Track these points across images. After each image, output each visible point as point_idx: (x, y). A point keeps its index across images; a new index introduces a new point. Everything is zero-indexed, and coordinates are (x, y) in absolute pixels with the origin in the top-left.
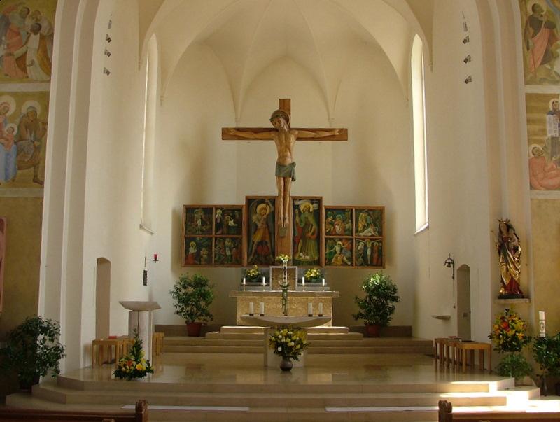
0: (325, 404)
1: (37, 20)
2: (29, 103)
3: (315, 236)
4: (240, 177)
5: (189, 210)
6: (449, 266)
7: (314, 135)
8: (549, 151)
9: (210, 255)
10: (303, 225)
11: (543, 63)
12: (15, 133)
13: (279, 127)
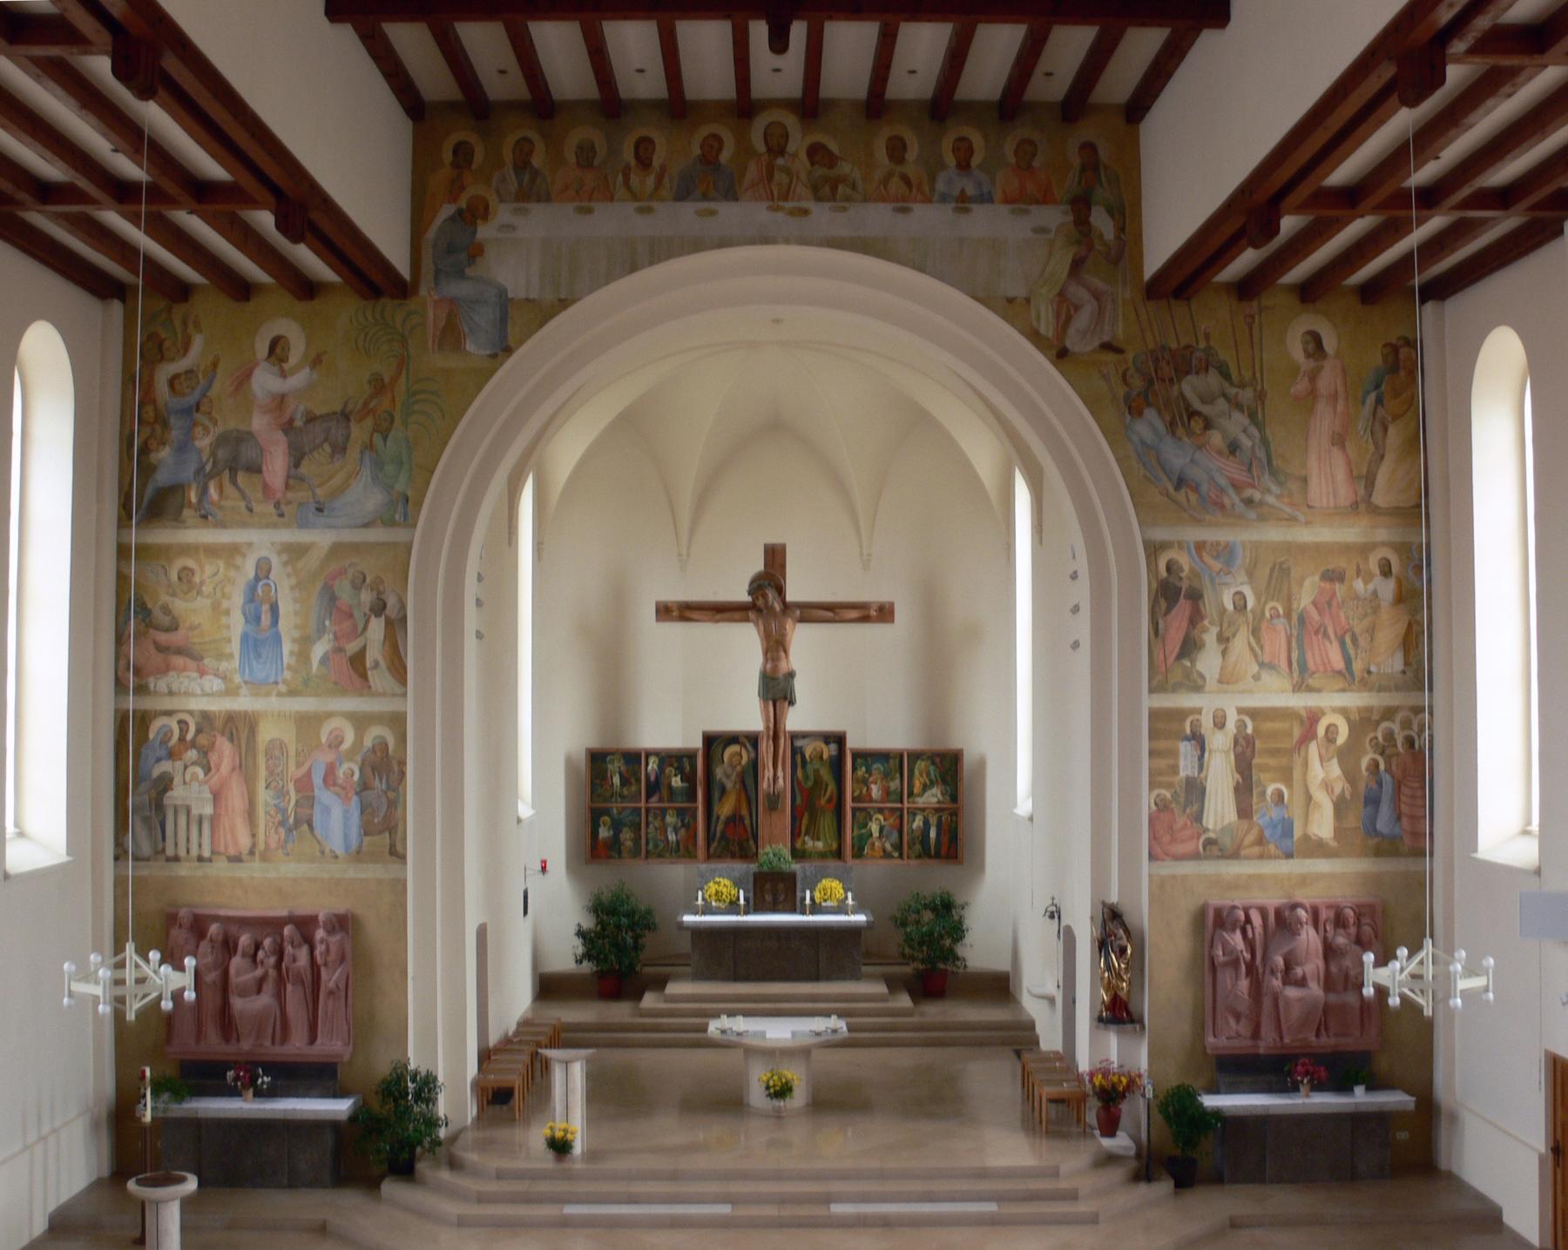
0: (828, 1199)
1: (379, 593)
4: (697, 692)
5: (597, 759)
8: (1182, 800)
9: (637, 840)
10: (810, 784)
13: (767, 602)
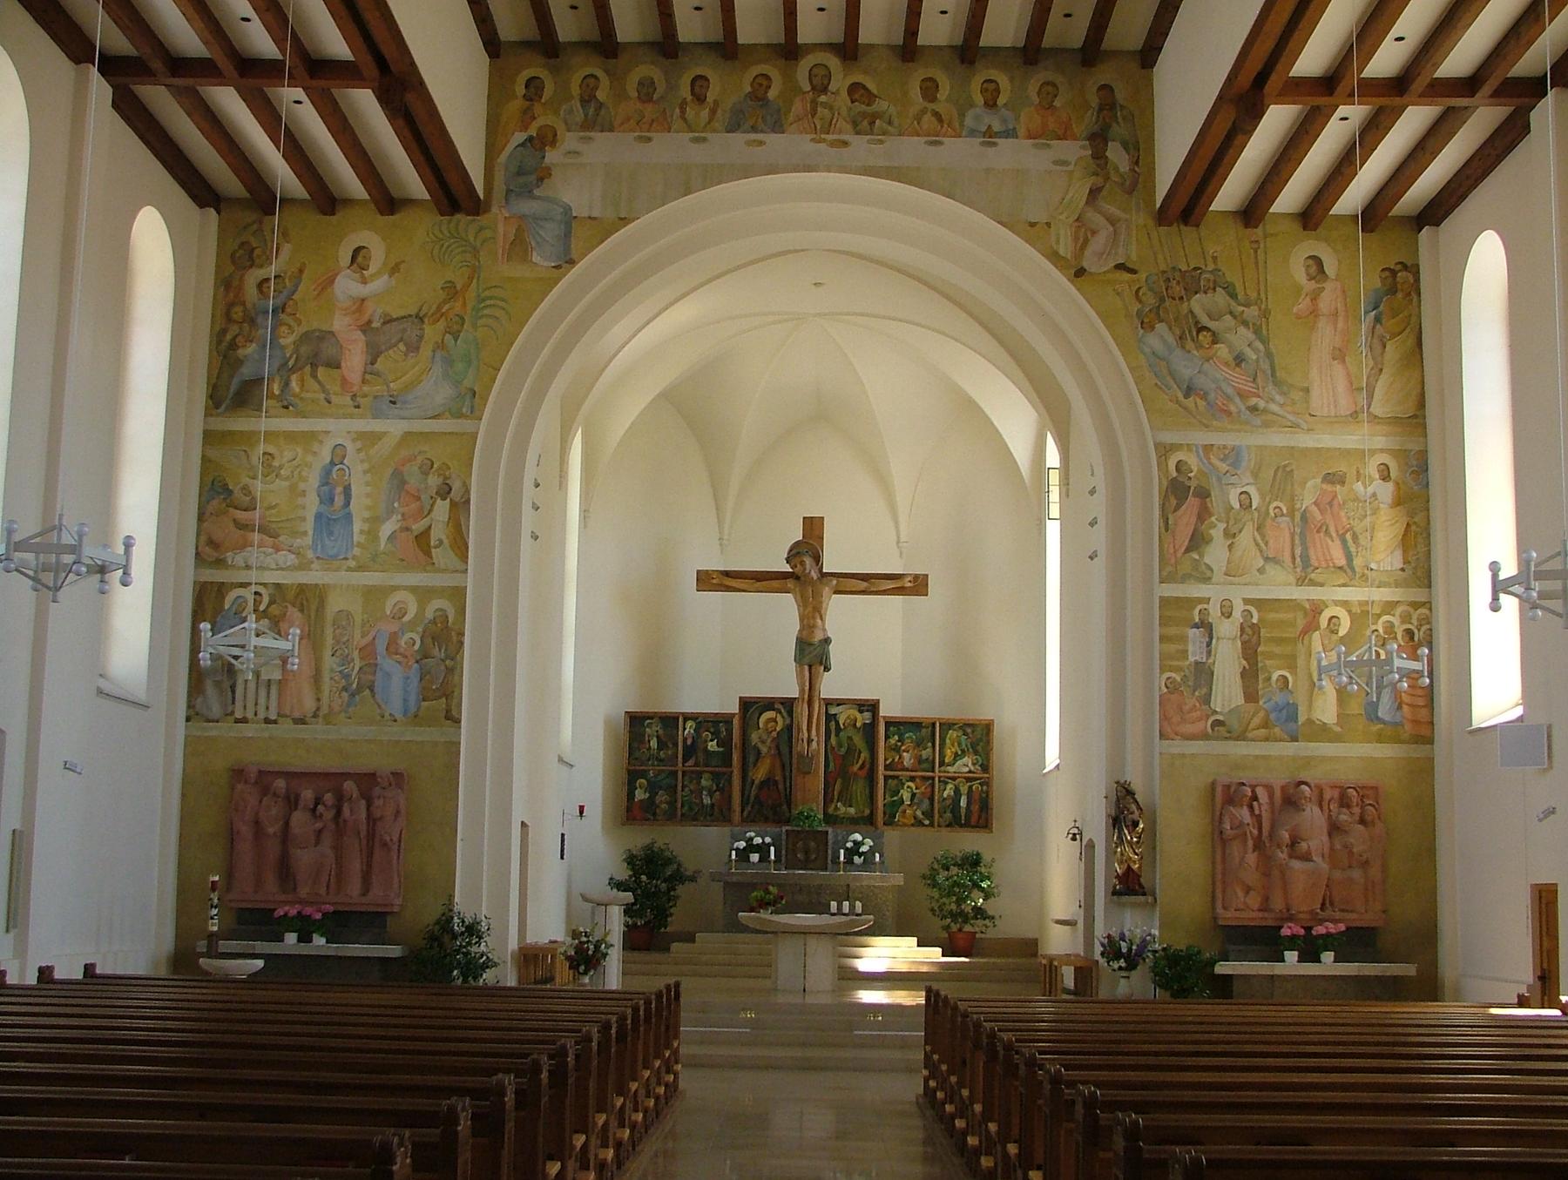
2: (437, 604)
3: (864, 773)
4: (734, 658)
5: (636, 721)
6: (1074, 839)
7: (868, 583)
9: (672, 803)
10: (843, 751)
11: (1188, 550)
12: (417, 647)
13: (804, 572)
